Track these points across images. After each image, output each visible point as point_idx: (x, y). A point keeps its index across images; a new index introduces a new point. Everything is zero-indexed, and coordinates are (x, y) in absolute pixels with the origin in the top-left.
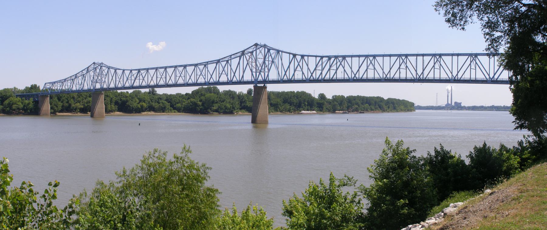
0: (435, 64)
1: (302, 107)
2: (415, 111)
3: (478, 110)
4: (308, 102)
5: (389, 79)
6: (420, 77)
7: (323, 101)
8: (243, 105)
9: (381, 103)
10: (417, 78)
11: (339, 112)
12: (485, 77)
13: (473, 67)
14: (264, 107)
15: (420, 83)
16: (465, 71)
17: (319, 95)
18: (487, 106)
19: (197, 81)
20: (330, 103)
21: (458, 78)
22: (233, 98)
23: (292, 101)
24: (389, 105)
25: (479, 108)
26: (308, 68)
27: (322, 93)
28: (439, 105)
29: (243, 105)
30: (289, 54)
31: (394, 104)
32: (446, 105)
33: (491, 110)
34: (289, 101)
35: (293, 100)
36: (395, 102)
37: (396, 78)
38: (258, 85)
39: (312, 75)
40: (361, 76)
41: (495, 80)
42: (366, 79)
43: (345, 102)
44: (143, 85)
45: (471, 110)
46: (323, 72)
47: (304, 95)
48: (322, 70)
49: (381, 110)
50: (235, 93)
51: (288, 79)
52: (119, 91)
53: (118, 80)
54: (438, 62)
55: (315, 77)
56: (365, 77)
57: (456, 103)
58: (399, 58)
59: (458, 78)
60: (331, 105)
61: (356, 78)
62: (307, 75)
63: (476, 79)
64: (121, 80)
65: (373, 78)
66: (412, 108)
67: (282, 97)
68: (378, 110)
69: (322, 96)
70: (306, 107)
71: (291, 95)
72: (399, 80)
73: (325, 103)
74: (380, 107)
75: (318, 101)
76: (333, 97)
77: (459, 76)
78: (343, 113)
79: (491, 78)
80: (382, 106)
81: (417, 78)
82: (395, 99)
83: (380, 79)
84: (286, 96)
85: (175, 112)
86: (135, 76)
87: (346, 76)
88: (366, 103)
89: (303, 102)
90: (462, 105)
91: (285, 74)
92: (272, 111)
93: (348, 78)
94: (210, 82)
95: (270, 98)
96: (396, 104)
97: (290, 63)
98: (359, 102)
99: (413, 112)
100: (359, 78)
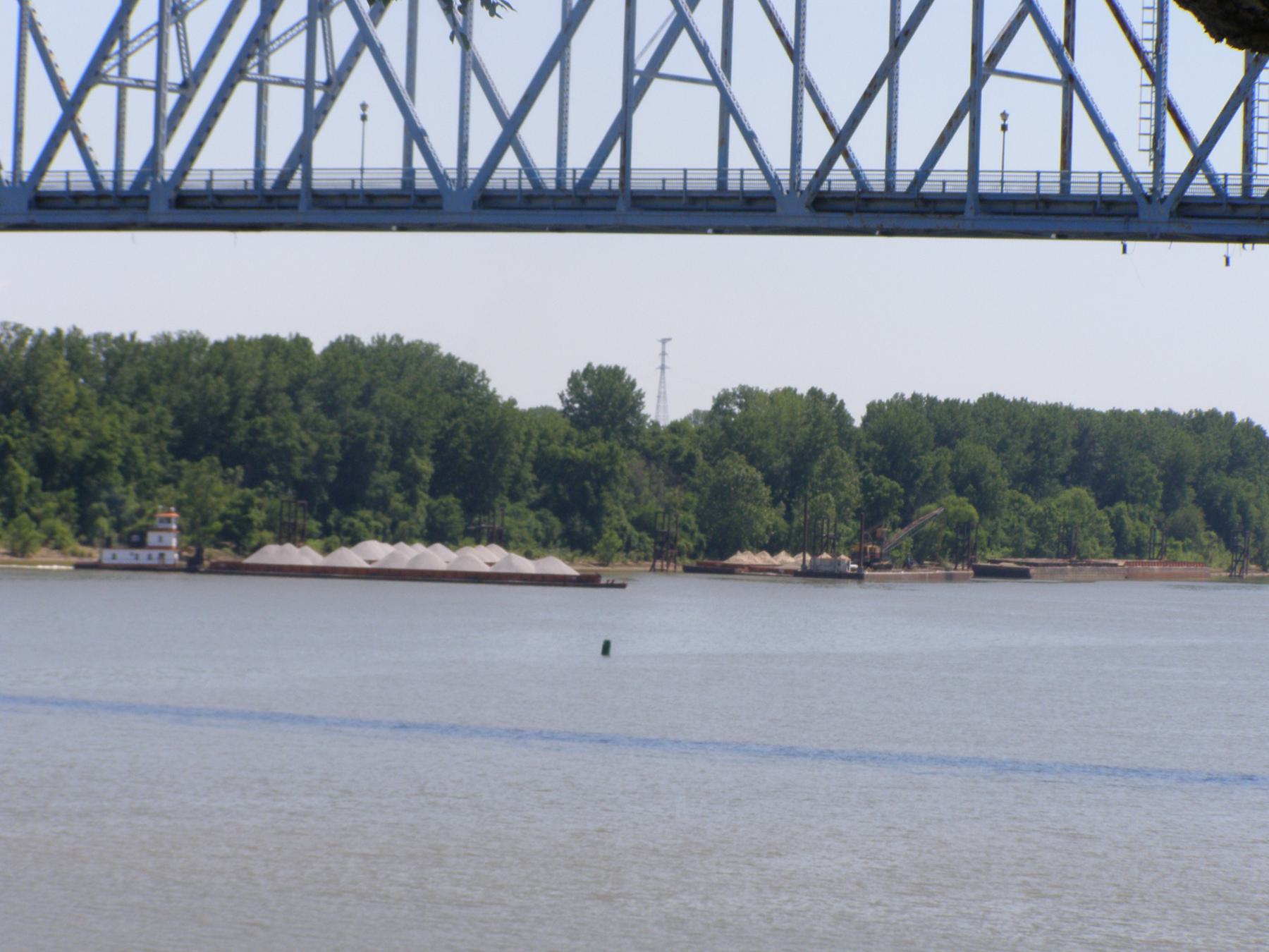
1: (381, 504)
4: (441, 451)
5: (1234, 204)
7: (602, 447)
9: (1230, 482)
11: (762, 559)
12: (1115, 168)
15: (1219, 249)
16: (1138, 64)
17: (574, 381)
20: (677, 468)
23: (271, 436)
26: (802, 83)
27: (604, 358)
34: (240, 437)
35: (277, 427)
39: (509, 137)
40: (909, 160)
43: (847, 459)
47: (406, 385)
48: (716, 81)
49: (1231, 546)
55: (544, 160)
60: (695, 489)
63: (733, 185)
67: (160, 390)
68: (1199, 547)
70: (424, 500)
71: (264, 380)
73: (630, 464)
75: (555, 447)
78: (807, 574)
80: (1243, 509)
81: (1167, 190)
83: (1130, 201)
84: (217, 386)
88: (1077, 473)
89: (385, 449)
91: (68, 123)
92: (51, 534)
93: (1114, 185)
94: (52, 181)
95: (37, 396)
98: (992, 462)
100: (890, 183)
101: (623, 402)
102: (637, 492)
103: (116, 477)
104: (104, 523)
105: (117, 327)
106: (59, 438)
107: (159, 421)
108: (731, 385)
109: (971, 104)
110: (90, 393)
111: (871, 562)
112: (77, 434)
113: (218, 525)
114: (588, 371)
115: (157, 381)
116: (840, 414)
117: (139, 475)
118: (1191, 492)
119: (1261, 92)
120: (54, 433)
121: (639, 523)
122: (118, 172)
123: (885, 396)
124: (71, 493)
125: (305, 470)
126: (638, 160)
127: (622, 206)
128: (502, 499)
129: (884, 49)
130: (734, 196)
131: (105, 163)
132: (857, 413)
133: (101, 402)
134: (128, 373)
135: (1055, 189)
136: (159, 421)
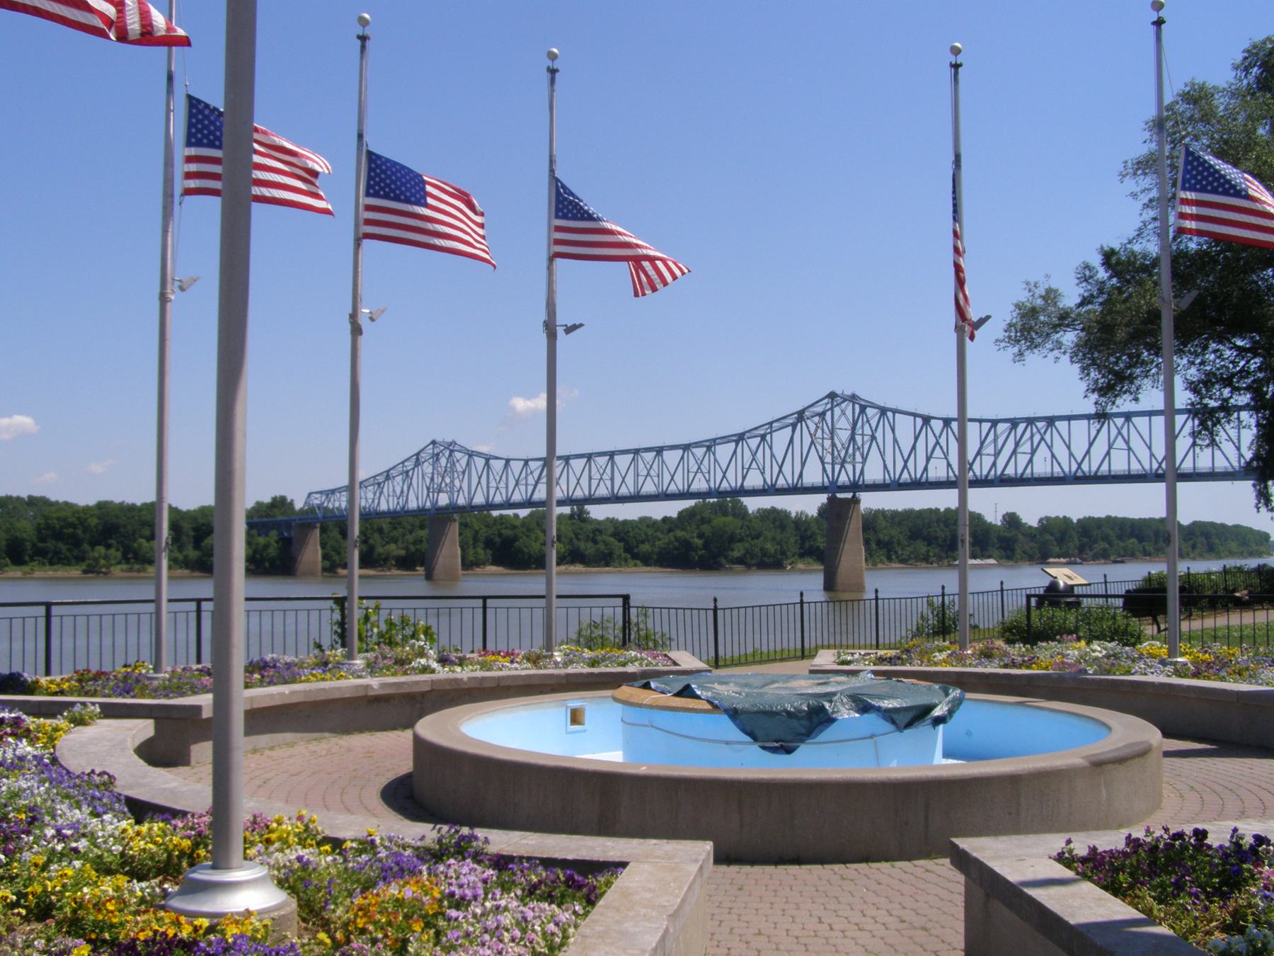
7: (1013, 533)
8: (807, 545)
11: (1056, 560)
14: (853, 551)
19: (689, 486)
22: (782, 527)
29: (807, 545)
30: (912, 418)
35: (935, 531)
38: (839, 495)
40: (1020, 471)
44: (516, 501)
51: (911, 479)
52: (495, 513)
53: (493, 484)
55: (978, 473)
61: (1083, 472)
64: (502, 485)
66: (1262, 549)
73: (1020, 537)
75: (1002, 534)
76: (1041, 520)
82: (1212, 524)
85: (635, 565)
86: (536, 474)
87: (1057, 469)
88: (1132, 535)
91: (905, 466)
94: (722, 489)
97: (916, 438)
98: (1111, 533)
103: (896, 545)
104: (894, 557)
106: (881, 536)
108: (1043, 516)
109: (1108, 453)
110: (888, 524)
111: (1085, 560)
114: (1007, 514)
115: (904, 520)
116: (1072, 521)
119: (1148, 450)
121: (1024, 552)
122: (1070, 471)
123: (1081, 517)
124: (885, 550)
126: (866, 478)
128: (990, 548)
129: (1087, 447)
131: (790, 482)
132: (1075, 521)
134: (897, 520)
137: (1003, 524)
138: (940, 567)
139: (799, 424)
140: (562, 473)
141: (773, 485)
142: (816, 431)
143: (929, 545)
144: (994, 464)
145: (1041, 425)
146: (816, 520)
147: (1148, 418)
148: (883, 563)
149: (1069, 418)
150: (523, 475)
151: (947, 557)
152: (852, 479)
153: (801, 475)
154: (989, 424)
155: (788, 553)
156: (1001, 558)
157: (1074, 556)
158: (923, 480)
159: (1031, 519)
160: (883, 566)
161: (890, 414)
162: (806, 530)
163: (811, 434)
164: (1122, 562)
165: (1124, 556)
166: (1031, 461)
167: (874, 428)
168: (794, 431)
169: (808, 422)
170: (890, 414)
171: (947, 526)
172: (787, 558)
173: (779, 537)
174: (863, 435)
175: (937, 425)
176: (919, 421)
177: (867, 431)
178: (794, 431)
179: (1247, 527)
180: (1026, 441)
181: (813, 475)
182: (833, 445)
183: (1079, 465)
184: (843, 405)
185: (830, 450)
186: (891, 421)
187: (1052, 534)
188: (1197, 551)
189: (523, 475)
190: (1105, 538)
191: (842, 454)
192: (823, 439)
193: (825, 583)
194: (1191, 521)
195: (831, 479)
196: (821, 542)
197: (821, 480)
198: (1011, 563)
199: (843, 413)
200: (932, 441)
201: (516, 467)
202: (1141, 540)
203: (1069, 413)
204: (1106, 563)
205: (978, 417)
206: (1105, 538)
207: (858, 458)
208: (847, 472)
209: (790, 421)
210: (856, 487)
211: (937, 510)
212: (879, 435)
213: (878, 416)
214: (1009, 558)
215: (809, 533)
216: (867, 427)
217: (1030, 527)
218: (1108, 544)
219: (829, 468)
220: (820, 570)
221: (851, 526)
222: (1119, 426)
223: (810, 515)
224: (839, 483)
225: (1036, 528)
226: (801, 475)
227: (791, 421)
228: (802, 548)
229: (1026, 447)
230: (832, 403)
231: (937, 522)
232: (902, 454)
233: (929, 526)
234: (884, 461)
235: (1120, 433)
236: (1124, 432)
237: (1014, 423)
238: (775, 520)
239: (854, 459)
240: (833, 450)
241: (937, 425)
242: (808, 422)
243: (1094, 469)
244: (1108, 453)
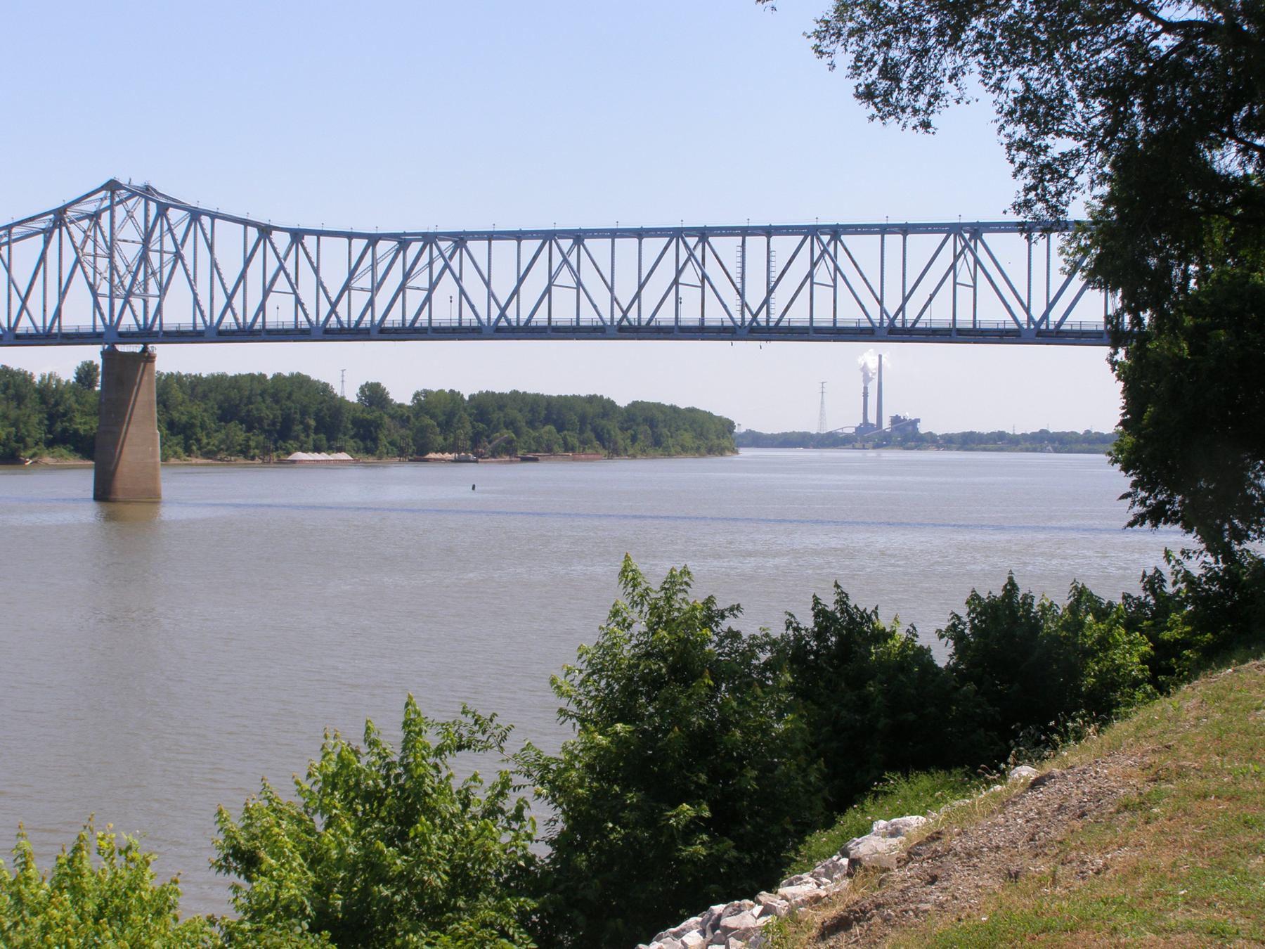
0: (814, 265)
1: (297, 438)
2: (737, 452)
3: (985, 450)
4: (319, 419)
6: (755, 316)
7: (377, 414)
8: (59, 427)
9: (604, 422)
10: (747, 324)
11: (439, 456)
13: (964, 275)
15: (758, 343)
18: (1018, 432)
21: (904, 321)
22: (19, 399)
24: (635, 427)
25: (986, 442)
26: (320, 283)
28: (830, 427)
30: (242, 226)
31: (656, 427)
32: (857, 429)
33: (1034, 450)
35: (257, 409)
36: (660, 416)
37: (662, 324)
38: (121, 348)
39: (333, 311)
40: (410, 317)
41: (1052, 327)
42: (190, 331)
45: (958, 450)
46: (1051, 314)
47: (303, 391)
48: (372, 291)
50: (25, 378)
51: (238, 324)
54: (827, 257)
55: (344, 318)
56: (541, 317)
57: (896, 420)
58: (809, 238)
59: (904, 321)
60: (410, 429)
61: (508, 321)
62: (315, 309)
65: (574, 324)
66: (725, 443)
67: (212, 395)
69: (374, 395)
70: (312, 436)
71: (251, 390)
72: (954, 334)
73: (386, 420)
74: (600, 438)
76: (417, 395)
77: (911, 314)
78: (456, 461)
79: (1037, 318)
80: (609, 433)
82: (659, 407)
84: (234, 394)
87: (468, 316)
88: (547, 420)
89: (298, 416)
90: (923, 429)
91: (229, 305)
92: (176, 453)
93: (475, 324)
95: (168, 399)
96: (661, 425)
97: (247, 262)
98: (519, 416)
99: (729, 459)
101: (382, 396)
102: (389, 431)
103: (198, 430)
104: (194, 448)
105: (194, 371)
106: (175, 415)
107: (212, 408)
109: (548, 291)
111: (481, 456)
112: (182, 414)
113: (238, 448)
115: (211, 391)
117: (206, 429)
118: (589, 426)
120: (174, 413)
121: (392, 443)
124: (181, 436)
125: (268, 425)
127: (811, 332)
128: (340, 436)
130: (466, 328)
133: (190, 400)
134: (200, 389)
135: (457, 325)
136: (212, 408)
137: (360, 399)
138: (266, 463)
139: (57, 231)
140: (535, 258)
141: (12, 329)
142: (84, 242)
143: (249, 429)
144: (371, 303)
145: (445, 245)
146: (72, 388)
147: (741, 238)
148: (179, 458)
149: (490, 236)
150: (166, 271)
151: (277, 449)
152: (141, 322)
153: (58, 313)
154: (365, 242)
155: (28, 439)
156: (357, 451)
157: (466, 451)
158: (258, 326)
159: (401, 394)
160: (178, 462)
161: (206, 220)
162: (57, 404)
163: (75, 248)
164: (535, 460)
165: (537, 451)
166: (428, 299)
167: (179, 242)
168: (47, 242)
169: (72, 227)
170: (206, 220)
171: (277, 402)
172: (26, 447)
173: (13, 414)
174: (161, 252)
175: (281, 240)
176: (253, 233)
177: (169, 246)
178: (47, 242)
179: (705, 412)
180: (422, 270)
181: (78, 315)
182: (113, 267)
183: (625, 313)
184: (131, 203)
185: (107, 275)
186: (208, 232)
187: (433, 417)
188: (638, 445)
189: (166, 271)
190: (510, 424)
191: (127, 283)
192: (95, 256)
193: (96, 490)
194: (630, 402)
195: (108, 321)
196: (84, 424)
197: (91, 323)
198: (371, 459)
199: (130, 215)
200: (273, 265)
201: (335, 257)
202: (560, 429)
203: (612, 225)
204: (511, 462)
205: (345, 228)
206: (510, 424)
207: (153, 288)
208: (133, 312)
209: (41, 224)
210: (148, 335)
211: (262, 377)
212: (187, 252)
213: (188, 220)
214: (369, 451)
215: (61, 409)
216: (168, 239)
217: (401, 406)
218: (514, 432)
219: (104, 303)
220: (88, 467)
221: (139, 398)
222: (825, 243)
223: (64, 379)
224: (122, 328)
225: (409, 407)
226: (58, 313)
227: (43, 226)
228: (50, 432)
229: (421, 280)
230: (112, 198)
231: (261, 395)
232: (223, 285)
233: (250, 401)
234: (195, 295)
235: (691, 255)
236: (573, 259)
237: (403, 241)
238: (7, 386)
239: (146, 290)
240: (112, 275)
241: (281, 240)
242: (72, 227)
243: (524, 316)
244: (548, 291)
